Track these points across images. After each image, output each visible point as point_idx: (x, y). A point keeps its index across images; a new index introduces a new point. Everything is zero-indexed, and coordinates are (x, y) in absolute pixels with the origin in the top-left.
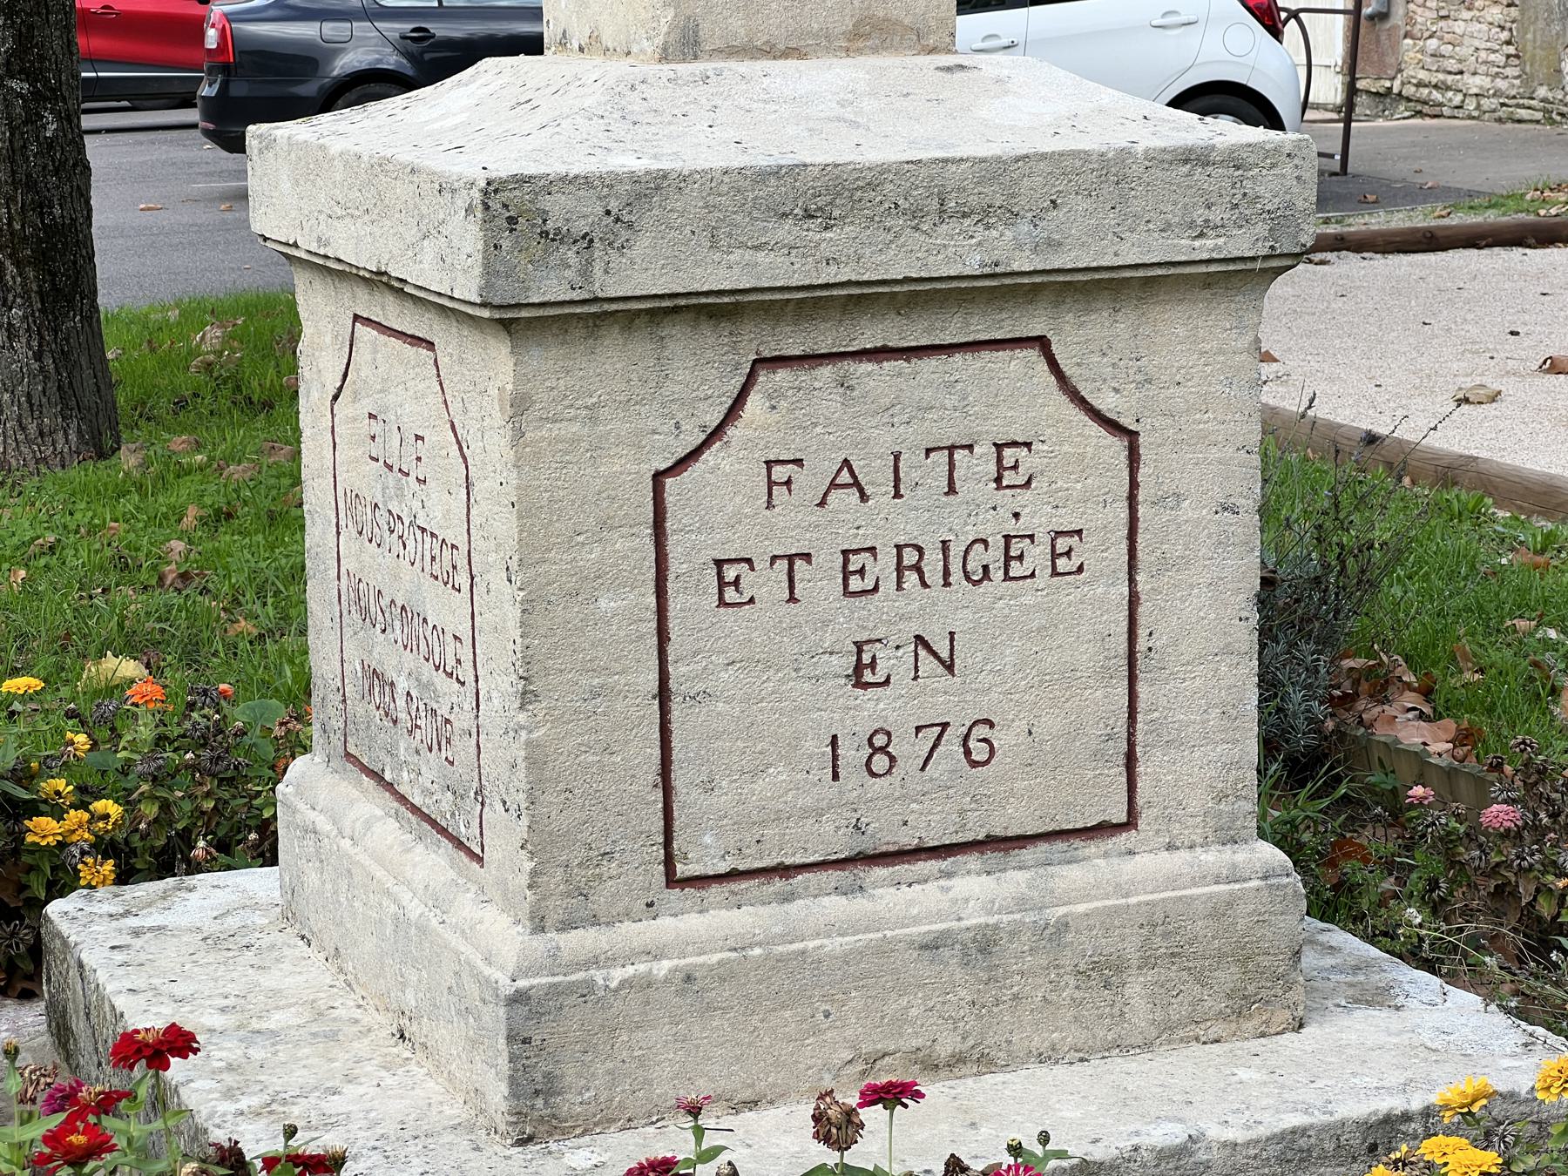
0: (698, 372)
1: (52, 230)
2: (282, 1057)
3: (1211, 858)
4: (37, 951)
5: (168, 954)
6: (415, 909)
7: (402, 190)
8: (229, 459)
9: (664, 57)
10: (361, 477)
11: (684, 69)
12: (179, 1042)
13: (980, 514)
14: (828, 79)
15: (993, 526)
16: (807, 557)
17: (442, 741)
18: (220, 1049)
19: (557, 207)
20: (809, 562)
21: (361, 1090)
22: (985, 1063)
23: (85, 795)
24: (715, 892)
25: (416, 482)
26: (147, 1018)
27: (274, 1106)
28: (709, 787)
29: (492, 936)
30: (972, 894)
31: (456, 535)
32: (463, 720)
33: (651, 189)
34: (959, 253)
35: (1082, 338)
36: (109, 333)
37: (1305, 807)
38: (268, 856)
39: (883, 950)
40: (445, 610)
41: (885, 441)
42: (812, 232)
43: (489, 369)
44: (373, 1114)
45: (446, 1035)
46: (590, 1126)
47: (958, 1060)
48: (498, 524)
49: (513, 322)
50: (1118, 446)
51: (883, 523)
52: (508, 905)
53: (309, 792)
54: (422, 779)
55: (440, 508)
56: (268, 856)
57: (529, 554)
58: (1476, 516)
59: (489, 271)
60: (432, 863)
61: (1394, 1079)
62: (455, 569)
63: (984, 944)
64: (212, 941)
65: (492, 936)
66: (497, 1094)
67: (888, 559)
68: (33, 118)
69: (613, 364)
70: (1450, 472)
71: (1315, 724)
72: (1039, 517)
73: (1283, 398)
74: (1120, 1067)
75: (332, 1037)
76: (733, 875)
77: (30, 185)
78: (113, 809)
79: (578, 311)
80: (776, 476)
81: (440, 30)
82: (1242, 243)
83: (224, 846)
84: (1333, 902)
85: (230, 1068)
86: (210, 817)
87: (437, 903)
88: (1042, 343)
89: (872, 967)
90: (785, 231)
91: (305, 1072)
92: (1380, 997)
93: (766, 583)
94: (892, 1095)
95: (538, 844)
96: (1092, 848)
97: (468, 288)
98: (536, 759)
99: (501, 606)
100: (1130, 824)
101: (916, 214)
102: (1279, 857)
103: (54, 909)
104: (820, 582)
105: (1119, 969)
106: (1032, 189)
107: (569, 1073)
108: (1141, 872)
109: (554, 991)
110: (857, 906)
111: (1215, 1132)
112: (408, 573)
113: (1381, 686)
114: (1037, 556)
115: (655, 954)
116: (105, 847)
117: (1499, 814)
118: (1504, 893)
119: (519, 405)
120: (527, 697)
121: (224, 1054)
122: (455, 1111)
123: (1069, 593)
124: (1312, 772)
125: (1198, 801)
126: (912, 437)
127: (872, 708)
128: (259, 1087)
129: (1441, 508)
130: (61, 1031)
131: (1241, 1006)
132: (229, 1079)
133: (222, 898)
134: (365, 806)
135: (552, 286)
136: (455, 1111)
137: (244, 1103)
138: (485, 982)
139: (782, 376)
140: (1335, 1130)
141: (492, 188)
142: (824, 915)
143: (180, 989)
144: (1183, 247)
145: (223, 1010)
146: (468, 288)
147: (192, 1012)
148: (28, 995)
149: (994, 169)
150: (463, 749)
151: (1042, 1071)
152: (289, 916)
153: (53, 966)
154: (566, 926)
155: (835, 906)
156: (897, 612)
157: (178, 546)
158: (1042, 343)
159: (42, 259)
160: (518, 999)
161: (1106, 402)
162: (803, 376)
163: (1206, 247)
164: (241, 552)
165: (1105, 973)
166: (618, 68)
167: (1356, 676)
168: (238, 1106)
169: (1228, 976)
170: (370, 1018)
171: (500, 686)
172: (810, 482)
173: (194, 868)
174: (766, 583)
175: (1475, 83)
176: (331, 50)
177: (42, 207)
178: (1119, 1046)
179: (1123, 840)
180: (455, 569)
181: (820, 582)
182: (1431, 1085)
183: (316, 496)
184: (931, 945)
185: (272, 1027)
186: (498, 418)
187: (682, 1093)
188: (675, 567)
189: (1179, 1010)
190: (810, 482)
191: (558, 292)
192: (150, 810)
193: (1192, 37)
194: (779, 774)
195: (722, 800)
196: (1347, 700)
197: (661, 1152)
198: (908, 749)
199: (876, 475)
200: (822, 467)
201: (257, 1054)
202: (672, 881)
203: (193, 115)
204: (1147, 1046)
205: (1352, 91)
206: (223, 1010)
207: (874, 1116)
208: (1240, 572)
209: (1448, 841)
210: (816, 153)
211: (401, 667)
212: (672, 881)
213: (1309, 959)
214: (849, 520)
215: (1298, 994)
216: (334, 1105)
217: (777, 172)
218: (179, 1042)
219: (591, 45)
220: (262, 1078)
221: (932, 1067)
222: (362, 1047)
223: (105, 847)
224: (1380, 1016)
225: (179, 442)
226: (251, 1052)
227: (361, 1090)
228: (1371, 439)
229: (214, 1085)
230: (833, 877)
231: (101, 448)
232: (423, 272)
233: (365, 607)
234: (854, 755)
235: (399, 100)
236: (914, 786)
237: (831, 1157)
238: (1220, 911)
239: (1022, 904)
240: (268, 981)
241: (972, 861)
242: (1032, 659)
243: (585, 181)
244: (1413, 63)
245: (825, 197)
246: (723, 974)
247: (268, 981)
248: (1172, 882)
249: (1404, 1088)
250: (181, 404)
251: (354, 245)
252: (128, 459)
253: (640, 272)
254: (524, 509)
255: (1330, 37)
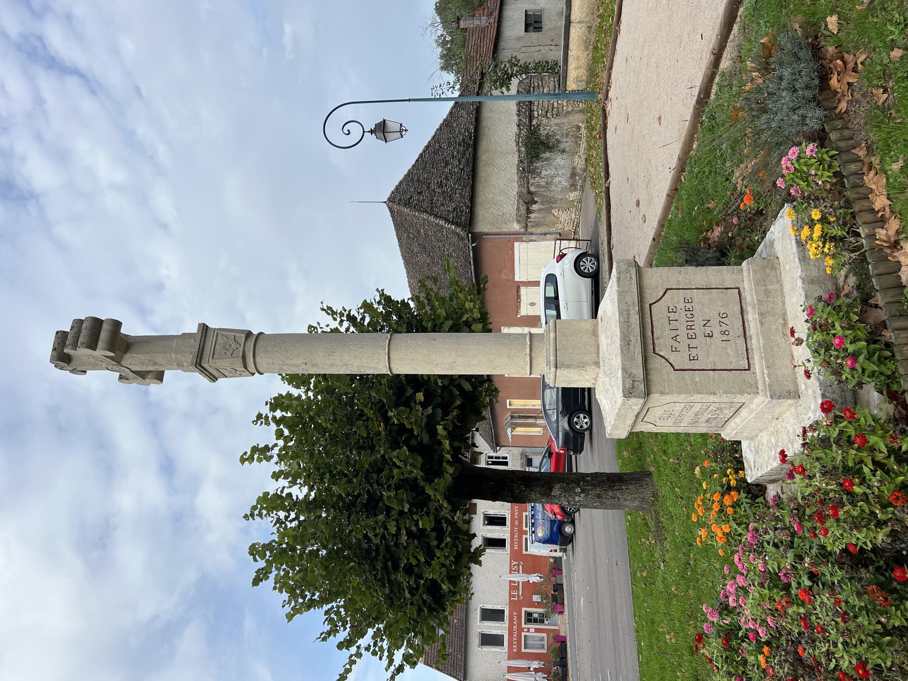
0: (656, 363)
1: (608, 480)
3: (745, 274)
4: (757, 485)
5: (759, 461)
6: (753, 415)
7: (622, 411)
8: (652, 450)
9: (599, 367)
10: (670, 422)
11: (601, 364)
12: (782, 453)
13: (681, 315)
14: (603, 340)
15: (683, 313)
17: (721, 409)
19: (628, 386)
22: (785, 314)
23: (726, 475)
24: (751, 362)
25: (674, 413)
26: (776, 463)
28: (731, 363)
29: (759, 401)
30: (751, 316)
31: (683, 405)
32: (717, 405)
33: (624, 370)
34: (635, 319)
35: (650, 298)
36: (625, 471)
37: (731, 254)
38: (739, 443)
39: (762, 332)
40: (697, 408)
41: (668, 332)
42: (632, 344)
43: (655, 397)
45: (777, 411)
46: (796, 385)
47: (784, 319)
48: (682, 397)
49: (648, 393)
50: (669, 292)
51: (683, 333)
52: (753, 399)
53: (728, 434)
54: (728, 413)
55: (678, 408)
56: (739, 443)
57: (688, 392)
58: (670, 221)
59: (639, 397)
60: (744, 412)
61: (788, 241)
62: (689, 405)
63: (761, 314)
64: (757, 453)
65: (759, 401)
66: (790, 401)
67: (689, 331)
68: (587, 481)
69: (653, 377)
70: (661, 225)
71: (715, 252)
72: (682, 305)
74: (785, 290)
75: (777, 431)
76: (748, 359)
77: (599, 483)
78: (729, 470)
80: (674, 350)
81: (560, 410)
82: (633, 271)
83: (736, 452)
84: (751, 250)
86: (731, 454)
87: (752, 411)
88: (650, 305)
89: (766, 334)
90: (632, 348)
92: (772, 243)
93: (694, 352)
94: (792, 332)
95: (742, 392)
96: (743, 295)
97: (642, 401)
98: (726, 393)
99: (697, 397)
100: (738, 288)
101: (628, 326)
102: (744, 263)
103: (749, 481)
104: (693, 343)
105: (766, 290)
106: (624, 307)
107: (786, 388)
108: (748, 287)
109: (770, 391)
110: (754, 337)
111: (799, 274)
112: (690, 414)
113: (706, 239)
114: (689, 306)
115: (763, 373)
116: (737, 472)
117: (735, 220)
118: (750, 219)
119: (662, 393)
120: (714, 394)
122: (793, 409)
123: (695, 300)
124: (724, 254)
125: (734, 277)
126: (667, 327)
127: (716, 334)
129: (668, 227)
130: (773, 481)
131: (774, 268)
133: (748, 451)
134: (732, 424)
135: (642, 387)
136: (793, 409)
138: (768, 403)
139: (656, 349)
140: (799, 252)
141: (625, 396)
142: (755, 343)
143: (766, 458)
144: (634, 281)
146: (642, 401)
148: (766, 488)
149: (621, 313)
150: (723, 405)
151: (787, 304)
152: (752, 439)
153: (761, 482)
154: (758, 388)
155: (754, 341)
156: (698, 329)
157: (671, 460)
158: (650, 305)
159: (614, 482)
160: (772, 397)
161: (661, 294)
162: (657, 345)
163: (634, 277)
164: (673, 448)
165: (767, 293)
166: (601, 375)
167: (705, 243)
169: (768, 271)
170: (773, 424)
171: (712, 398)
172: (675, 344)
173: (741, 456)
174: (694, 352)
175: (573, 216)
176: (564, 429)
177: (604, 481)
178: (782, 290)
179: (741, 290)
180: (689, 405)
181: (693, 343)
182: (790, 235)
183: (673, 430)
184: (762, 324)
186: (664, 397)
188: (691, 367)
189: (775, 279)
190: (675, 344)
191: (642, 385)
192: (729, 464)
193: (566, 270)
194: (729, 350)
195: (734, 360)
196: (709, 245)
197: (803, 372)
198: (724, 328)
199: (674, 333)
200: (673, 342)
202: (749, 369)
203: (573, 457)
204: (781, 285)
205: (574, 239)
207: (796, 335)
208: (691, 270)
209: (740, 229)
210: (618, 342)
211: (707, 416)
212: (749, 369)
213: (764, 255)
214: (682, 337)
215: (772, 258)
216: (791, 431)
217: (622, 349)
218: (782, 453)
219: (595, 379)
221: (785, 324)
222: (779, 426)
223: (737, 472)
224: (776, 243)
225: (648, 460)
228: (654, 239)
230: (748, 341)
231: (650, 474)
232: (637, 409)
233: (694, 423)
234: (725, 338)
235: (603, 412)
236: (731, 327)
237: (805, 343)
238: (755, 272)
239: (754, 308)
240: (765, 442)
241: (745, 317)
242: (708, 307)
243: (623, 381)
244: (569, 228)
245: (626, 341)
246: (767, 361)
247: (765, 442)
248: (750, 281)
249: (791, 240)
250: (640, 459)
251: (630, 422)
252: (652, 469)
253: (639, 372)
254: (680, 393)
255: (565, 244)
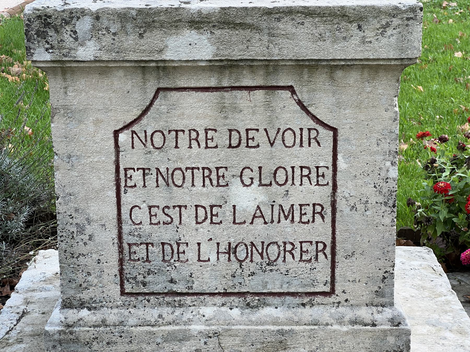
2: (427, 313)
16: (186, 207)
18: (449, 320)
20: (186, 209)
21: (404, 294)
27: (433, 297)
44: (403, 285)
73: (319, 51)
79: (382, 63)
85: (446, 312)
91: (420, 305)
121: (448, 318)
128: (437, 303)
132: (447, 308)
137: (443, 298)
145: (445, 338)
147: (458, 340)
158: (291, 89)
168: (445, 298)
185: (428, 327)
187: (338, 269)
201: (436, 316)
206: (445, 338)
220: (436, 306)
226: (438, 317)
227: (404, 294)
229: (453, 307)
